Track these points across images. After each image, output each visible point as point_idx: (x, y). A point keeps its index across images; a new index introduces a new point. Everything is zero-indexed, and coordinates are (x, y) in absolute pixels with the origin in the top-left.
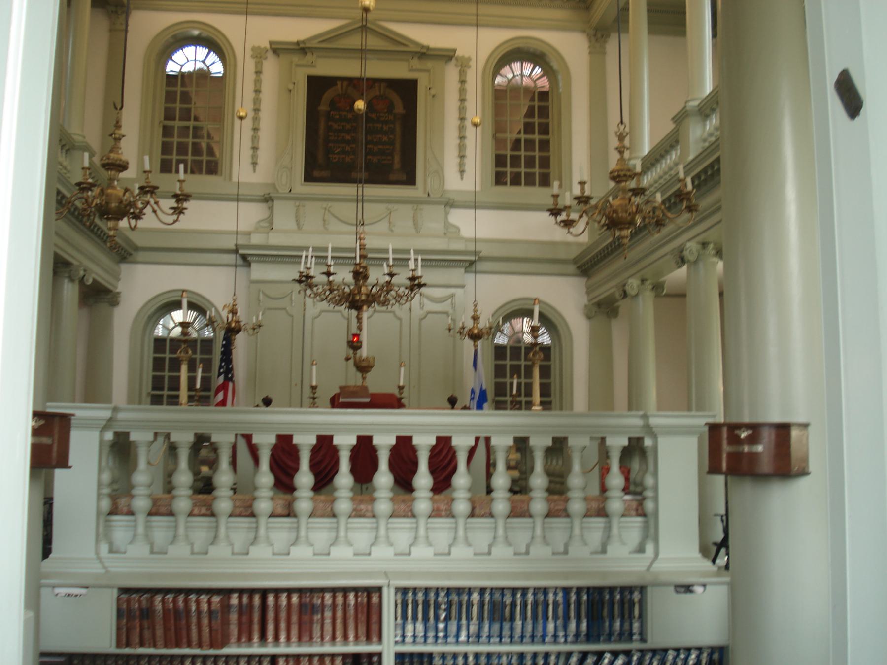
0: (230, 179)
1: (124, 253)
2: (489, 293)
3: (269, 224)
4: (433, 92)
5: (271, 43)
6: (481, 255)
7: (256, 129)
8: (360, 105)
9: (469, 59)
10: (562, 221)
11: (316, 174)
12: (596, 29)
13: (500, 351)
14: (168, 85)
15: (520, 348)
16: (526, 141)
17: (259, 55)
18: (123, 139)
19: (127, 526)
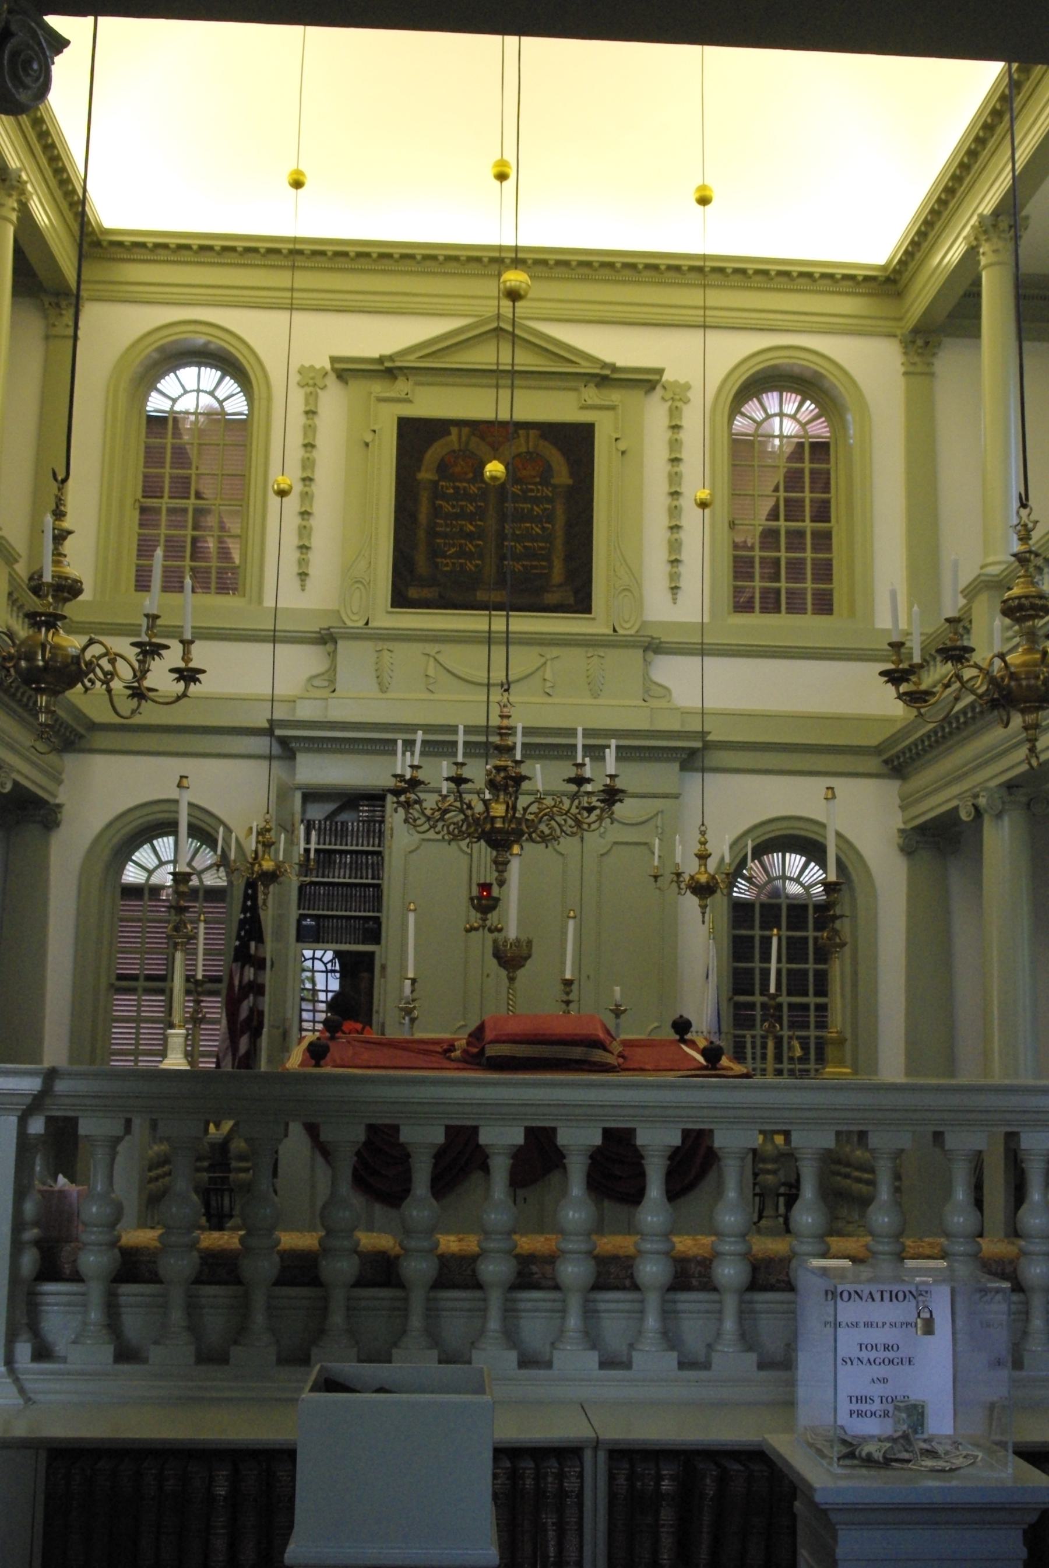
0: (260, 601)
1: (71, 737)
2: (731, 806)
3: (330, 678)
4: (622, 446)
5: (334, 360)
6: (709, 738)
7: (305, 514)
8: (495, 468)
9: (687, 387)
10: (905, 694)
11: (413, 593)
12: (916, 331)
13: (741, 911)
14: (150, 433)
15: (779, 907)
16: (788, 532)
18: (70, 537)
19: (69, 1304)
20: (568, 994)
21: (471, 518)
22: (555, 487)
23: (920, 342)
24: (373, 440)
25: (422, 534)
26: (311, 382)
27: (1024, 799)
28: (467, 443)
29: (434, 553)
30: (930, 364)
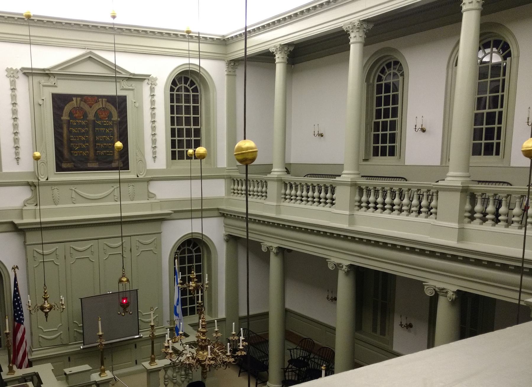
2: (176, 232)
11: (64, 166)
21: (83, 134)
22: (113, 121)
23: (232, 64)
24: (43, 103)
25: (65, 142)
26: (12, 75)
28: (80, 105)
29: (71, 149)
30: (234, 72)
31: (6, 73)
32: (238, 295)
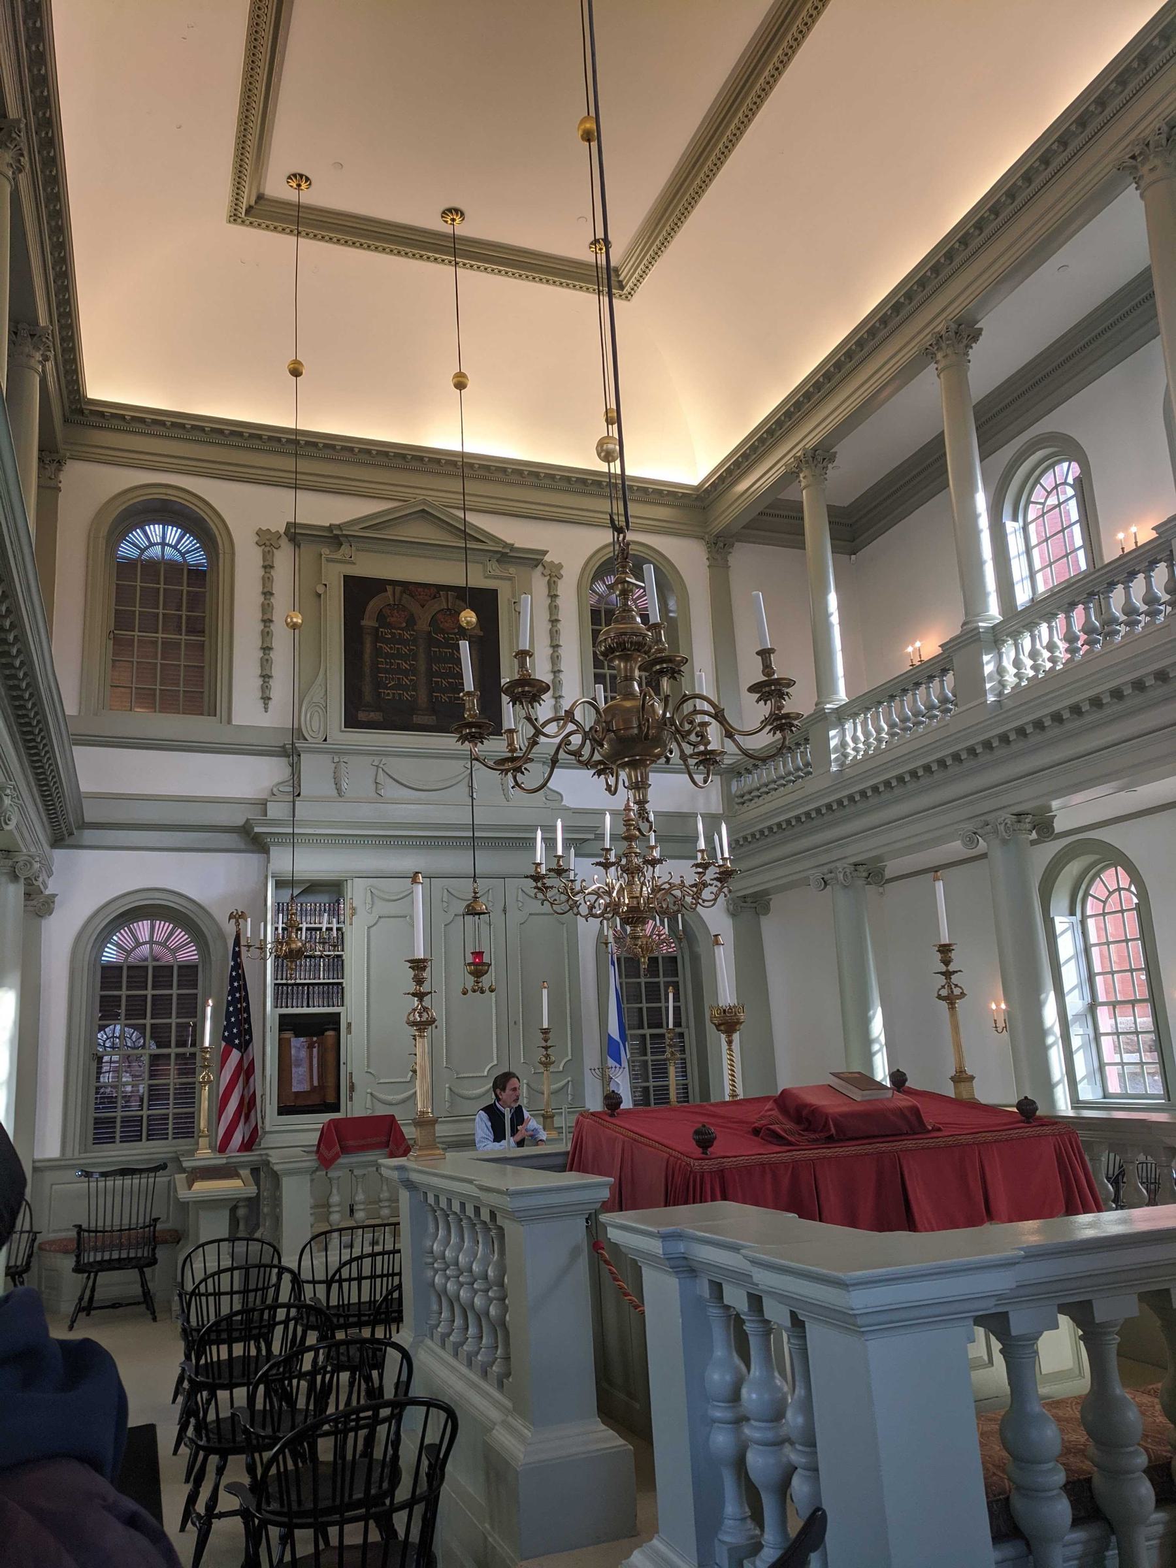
11: (362, 716)
17: (267, 541)
20: (546, 1041)
25: (367, 670)
27: (865, 874)
28: (400, 600)
31: (256, 538)
32: (771, 1029)
